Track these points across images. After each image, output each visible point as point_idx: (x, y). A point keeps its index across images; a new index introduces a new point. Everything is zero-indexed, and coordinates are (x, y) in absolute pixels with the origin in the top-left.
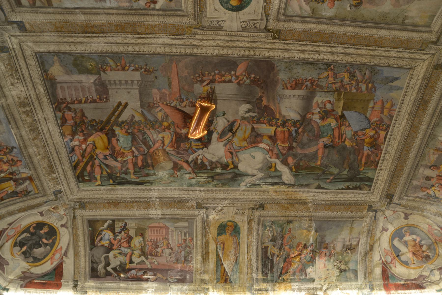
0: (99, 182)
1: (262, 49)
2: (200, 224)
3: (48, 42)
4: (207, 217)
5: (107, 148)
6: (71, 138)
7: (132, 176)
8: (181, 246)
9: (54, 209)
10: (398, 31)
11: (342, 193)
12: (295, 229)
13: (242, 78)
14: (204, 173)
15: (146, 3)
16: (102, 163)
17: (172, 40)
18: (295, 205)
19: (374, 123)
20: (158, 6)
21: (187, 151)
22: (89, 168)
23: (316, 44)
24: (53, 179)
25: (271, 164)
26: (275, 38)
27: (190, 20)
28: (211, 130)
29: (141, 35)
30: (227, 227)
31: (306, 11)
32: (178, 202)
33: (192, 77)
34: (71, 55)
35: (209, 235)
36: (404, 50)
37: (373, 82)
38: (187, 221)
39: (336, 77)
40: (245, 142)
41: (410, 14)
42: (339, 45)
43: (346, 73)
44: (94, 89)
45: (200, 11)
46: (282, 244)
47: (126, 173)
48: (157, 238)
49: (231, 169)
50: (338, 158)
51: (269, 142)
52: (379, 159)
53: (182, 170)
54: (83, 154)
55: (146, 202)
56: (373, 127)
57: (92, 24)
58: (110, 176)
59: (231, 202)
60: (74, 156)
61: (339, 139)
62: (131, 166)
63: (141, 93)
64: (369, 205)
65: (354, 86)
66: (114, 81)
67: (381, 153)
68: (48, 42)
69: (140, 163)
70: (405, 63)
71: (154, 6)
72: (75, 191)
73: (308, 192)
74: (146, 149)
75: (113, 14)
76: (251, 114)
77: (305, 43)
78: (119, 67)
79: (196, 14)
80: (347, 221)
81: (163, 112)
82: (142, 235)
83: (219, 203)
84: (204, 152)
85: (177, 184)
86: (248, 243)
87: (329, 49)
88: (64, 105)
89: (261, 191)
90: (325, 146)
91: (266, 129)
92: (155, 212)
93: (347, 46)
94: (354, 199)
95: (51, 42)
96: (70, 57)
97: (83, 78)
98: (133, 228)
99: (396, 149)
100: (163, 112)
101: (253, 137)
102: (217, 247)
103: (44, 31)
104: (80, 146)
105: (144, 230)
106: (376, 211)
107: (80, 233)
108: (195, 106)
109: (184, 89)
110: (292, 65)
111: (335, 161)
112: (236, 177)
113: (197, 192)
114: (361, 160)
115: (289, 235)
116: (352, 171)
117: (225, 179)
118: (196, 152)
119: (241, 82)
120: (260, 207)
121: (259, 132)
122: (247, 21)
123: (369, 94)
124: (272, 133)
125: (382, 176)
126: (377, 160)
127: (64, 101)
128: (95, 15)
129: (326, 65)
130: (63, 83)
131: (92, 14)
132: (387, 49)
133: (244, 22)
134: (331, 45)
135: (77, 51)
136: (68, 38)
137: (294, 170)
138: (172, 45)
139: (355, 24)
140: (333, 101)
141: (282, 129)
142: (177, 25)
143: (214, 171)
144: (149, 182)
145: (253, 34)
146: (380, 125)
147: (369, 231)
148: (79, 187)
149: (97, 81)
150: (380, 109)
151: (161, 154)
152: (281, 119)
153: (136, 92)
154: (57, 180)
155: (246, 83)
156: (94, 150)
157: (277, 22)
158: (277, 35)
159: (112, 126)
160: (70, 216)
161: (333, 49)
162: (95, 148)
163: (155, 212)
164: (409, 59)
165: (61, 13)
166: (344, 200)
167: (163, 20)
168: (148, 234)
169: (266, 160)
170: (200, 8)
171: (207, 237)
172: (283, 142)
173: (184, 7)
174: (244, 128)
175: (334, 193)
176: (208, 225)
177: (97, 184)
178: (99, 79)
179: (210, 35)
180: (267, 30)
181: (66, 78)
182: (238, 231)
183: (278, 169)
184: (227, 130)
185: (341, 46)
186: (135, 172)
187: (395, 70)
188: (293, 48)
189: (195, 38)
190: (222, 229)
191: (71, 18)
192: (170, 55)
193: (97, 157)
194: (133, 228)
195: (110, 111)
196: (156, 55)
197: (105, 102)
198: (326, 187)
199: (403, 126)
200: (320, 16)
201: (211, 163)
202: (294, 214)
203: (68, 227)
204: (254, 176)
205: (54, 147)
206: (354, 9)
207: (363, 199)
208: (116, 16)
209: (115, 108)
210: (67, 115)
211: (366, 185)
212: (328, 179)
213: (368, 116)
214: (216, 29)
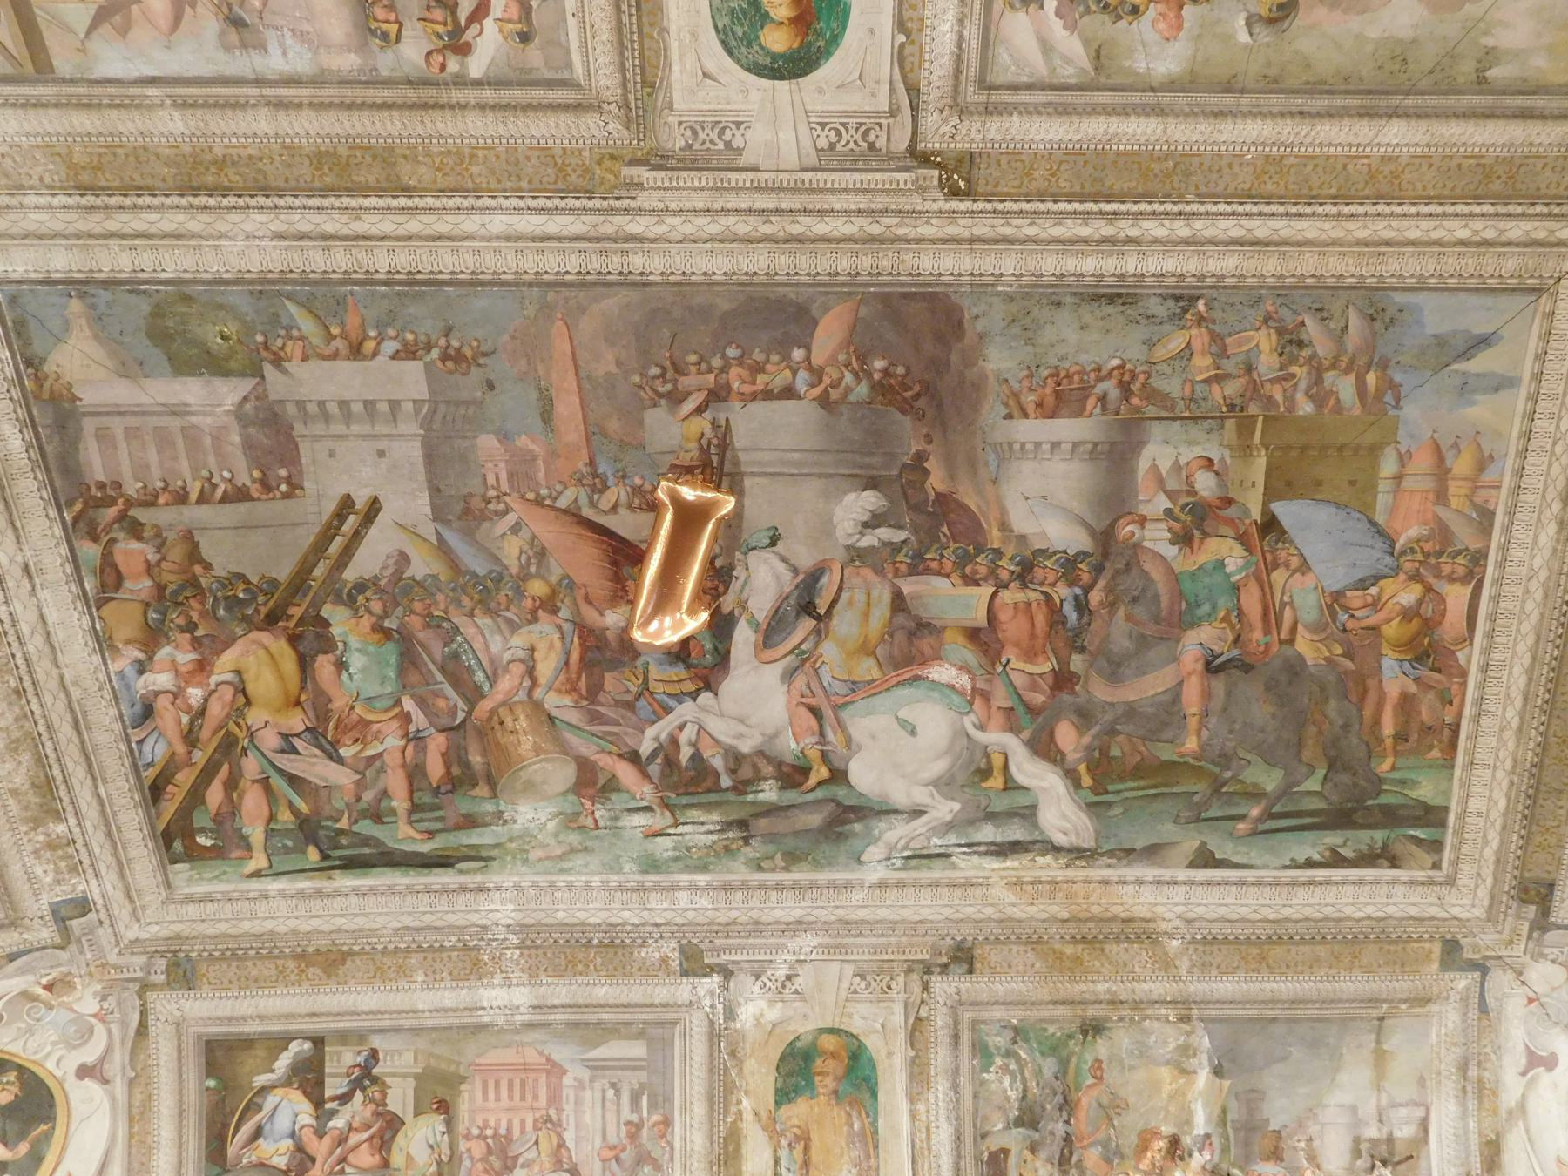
0: (259, 861)
1: (908, 241)
2: (699, 1049)
3: (41, 237)
4: (730, 1014)
5: (298, 703)
6: (141, 656)
7: (404, 830)
8: (617, 1159)
9: (49, 987)
10: (1462, 122)
11: (1312, 883)
12: (1121, 1062)
13: (835, 376)
14: (708, 807)
15: (429, 54)
16: (272, 773)
17: (543, 218)
18: (1107, 947)
19: (1413, 551)
20: (477, 66)
21: (630, 706)
22: (215, 794)
23: (1123, 208)
24: (51, 846)
25: (987, 756)
26: (955, 193)
27: (610, 127)
28: (726, 609)
29: (417, 200)
30: (819, 1062)
31: (1067, 60)
32: (601, 944)
33: (636, 379)
34: (138, 292)
35: (739, 1102)
36: (1501, 209)
37: (1384, 365)
38: (641, 1035)
39: (1223, 353)
40: (870, 663)
41: (1504, 39)
42: (1222, 207)
43: (1263, 332)
44: (236, 439)
45: (643, 82)
46: (1067, 1139)
47: (377, 818)
48: (510, 1121)
49: (820, 783)
50: (1274, 716)
51: (970, 655)
52: (1460, 715)
53: (614, 797)
54: (190, 731)
55: (466, 948)
56: (1408, 566)
57: (219, 151)
58: (308, 830)
59: (827, 940)
60: (150, 742)
61: (1267, 632)
62: (396, 782)
63: (429, 458)
64: (1445, 942)
65: (1303, 385)
66: (322, 404)
67: (1464, 684)
68: (41, 237)
69: (435, 769)
70: (1511, 264)
71: (462, 64)
72: (158, 904)
73: (1158, 883)
74: (461, 704)
75: (300, 105)
76: (884, 533)
77: (1077, 206)
78: (339, 344)
79: (631, 97)
80: (1354, 1019)
81: (525, 534)
82: (444, 1107)
83: (778, 948)
84: (702, 709)
85: (595, 861)
86: (913, 1135)
87: (1181, 229)
88: (112, 512)
89: (953, 885)
90: (1212, 666)
91: (953, 600)
92: (503, 997)
93: (1255, 209)
94: (1370, 910)
95: (53, 237)
96: (133, 299)
97: (191, 391)
98: (404, 1076)
99: (1527, 660)
100: (525, 534)
101: (900, 637)
102: (777, 1162)
103: (23, 187)
104: (177, 694)
105: (454, 1081)
106: (1482, 968)
107: (165, 1104)
108: (654, 507)
109: (605, 434)
110: (1036, 310)
111: (1262, 730)
112: (843, 823)
113: (683, 897)
114: (1377, 722)
115: (1095, 1092)
116: (1345, 778)
117: (796, 833)
118: (668, 711)
119: (834, 395)
120: (955, 959)
121: (924, 615)
122: (836, 122)
123: (1373, 418)
124: (981, 618)
125: (1482, 792)
126: (1448, 719)
127: (110, 493)
128: (229, 112)
129: (1177, 298)
130: (108, 414)
131: (215, 105)
132: (1424, 209)
133: (823, 125)
134: (1188, 208)
135: (164, 276)
136: (125, 217)
137: (1087, 781)
138: (547, 238)
139: (1276, 102)
140: (1222, 460)
141: (1020, 596)
142: (558, 151)
143: (750, 797)
144: (475, 855)
145: (864, 176)
146: (1440, 554)
147: (1463, 1068)
148: (168, 885)
149: (248, 406)
150: (1429, 484)
151: (523, 723)
152: (1010, 551)
153: (411, 451)
154: (70, 850)
155: (852, 398)
156: (240, 713)
157: (955, 120)
158: (960, 176)
159: (316, 605)
160: (124, 1024)
161: (1198, 224)
162: (242, 700)
163: (503, 997)
164: (1526, 245)
165: (88, 106)
166: (1326, 919)
167: (501, 130)
168: (468, 1102)
169: (965, 741)
170: (643, 69)
171: (733, 1109)
172: (1030, 655)
173: (579, 70)
174: (860, 597)
175: (1276, 883)
176: (733, 1054)
177: (251, 866)
178: (257, 398)
179: (692, 190)
180: (919, 157)
181: (122, 393)
182: (866, 1080)
183: (1021, 779)
184: (790, 608)
185: (1229, 209)
186: (415, 808)
187: (1475, 300)
188: (1032, 231)
189: (633, 204)
190: (797, 1068)
191: (131, 126)
192: (542, 284)
193: (252, 741)
194: (404, 1076)
195: (307, 538)
196: (482, 284)
197: (286, 496)
198: (1237, 859)
199: (1547, 553)
200: (1130, 80)
201: (736, 759)
202: (1109, 991)
203: (108, 1075)
204: (917, 813)
205: (62, 695)
206: (1264, 34)
207: (1413, 911)
208: (312, 113)
209: (329, 526)
210: (126, 553)
211: (1418, 842)
212: (1242, 817)
213: (1380, 518)
214: (714, 164)
